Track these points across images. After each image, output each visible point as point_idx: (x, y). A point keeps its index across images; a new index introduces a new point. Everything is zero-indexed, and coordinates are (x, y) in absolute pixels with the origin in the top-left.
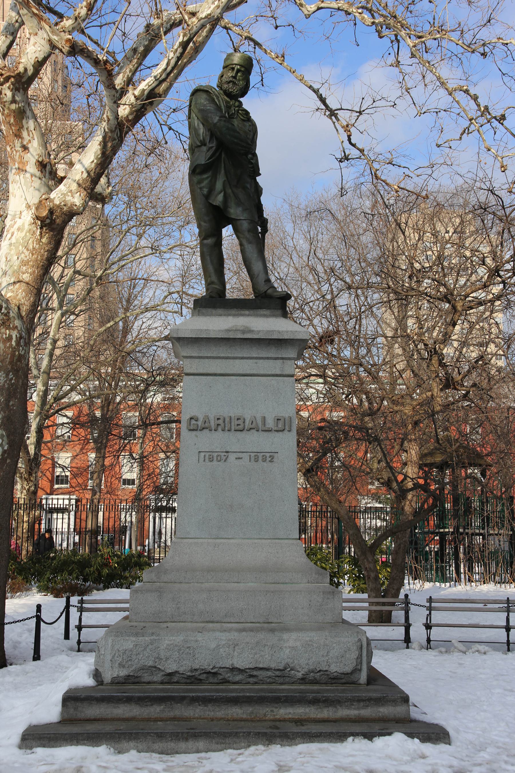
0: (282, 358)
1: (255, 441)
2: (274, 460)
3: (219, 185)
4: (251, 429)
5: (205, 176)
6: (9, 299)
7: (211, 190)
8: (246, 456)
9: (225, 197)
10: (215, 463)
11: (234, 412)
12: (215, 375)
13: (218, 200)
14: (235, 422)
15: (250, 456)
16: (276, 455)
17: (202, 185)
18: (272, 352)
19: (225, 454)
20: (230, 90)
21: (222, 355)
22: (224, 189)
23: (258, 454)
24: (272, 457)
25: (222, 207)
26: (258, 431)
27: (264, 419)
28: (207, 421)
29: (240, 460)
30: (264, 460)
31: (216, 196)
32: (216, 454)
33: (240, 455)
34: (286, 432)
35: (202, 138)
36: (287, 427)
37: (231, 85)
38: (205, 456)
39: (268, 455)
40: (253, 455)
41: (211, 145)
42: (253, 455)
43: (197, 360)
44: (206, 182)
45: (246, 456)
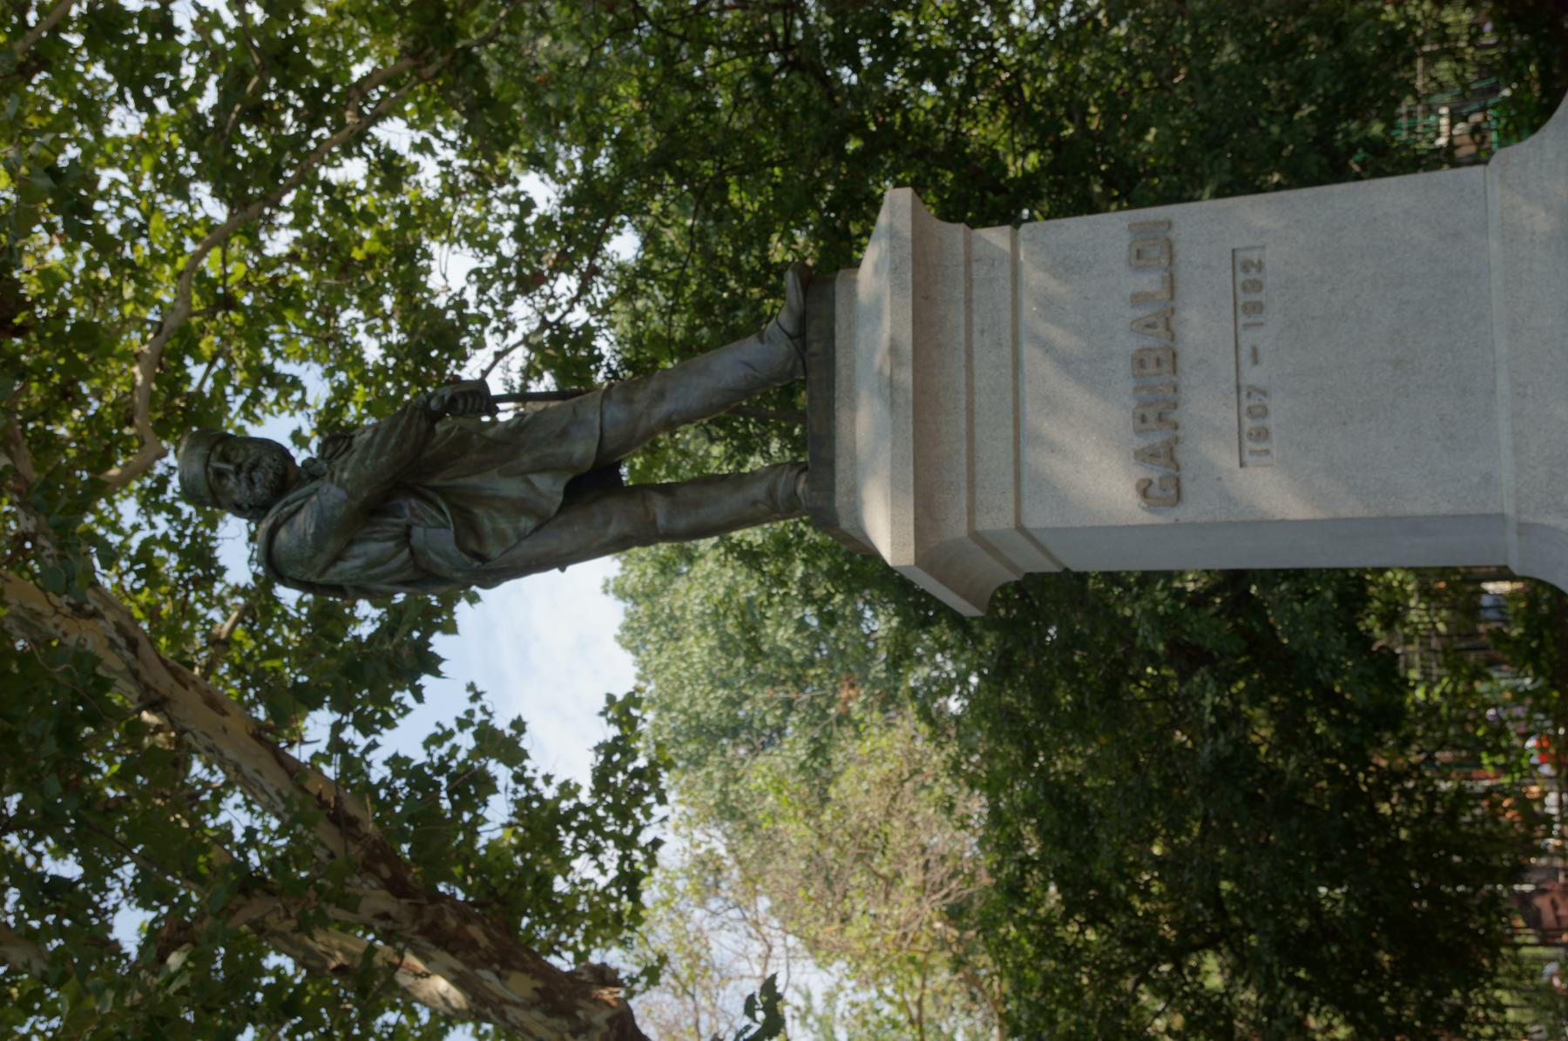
0: (968, 263)
1: (1202, 325)
3: (511, 488)
4: (1168, 328)
5: (487, 526)
6: (807, 954)
7: (521, 507)
8: (1247, 339)
9: (542, 467)
10: (1271, 422)
13: (550, 487)
15: (1246, 326)
16: (1240, 256)
17: (510, 532)
19: (1244, 394)
20: (271, 476)
21: (963, 425)
22: (524, 474)
23: (1240, 303)
24: (1246, 266)
25: (569, 477)
26: (1173, 311)
27: (1138, 299)
30: (1257, 286)
32: (1239, 292)
34: (1172, 235)
35: (391, 544)
37: (257, 475)
39: (1241, 277)
40: (1242, 319)
41: (407, 512)
42: (1242, 319)
44: (504, 525)
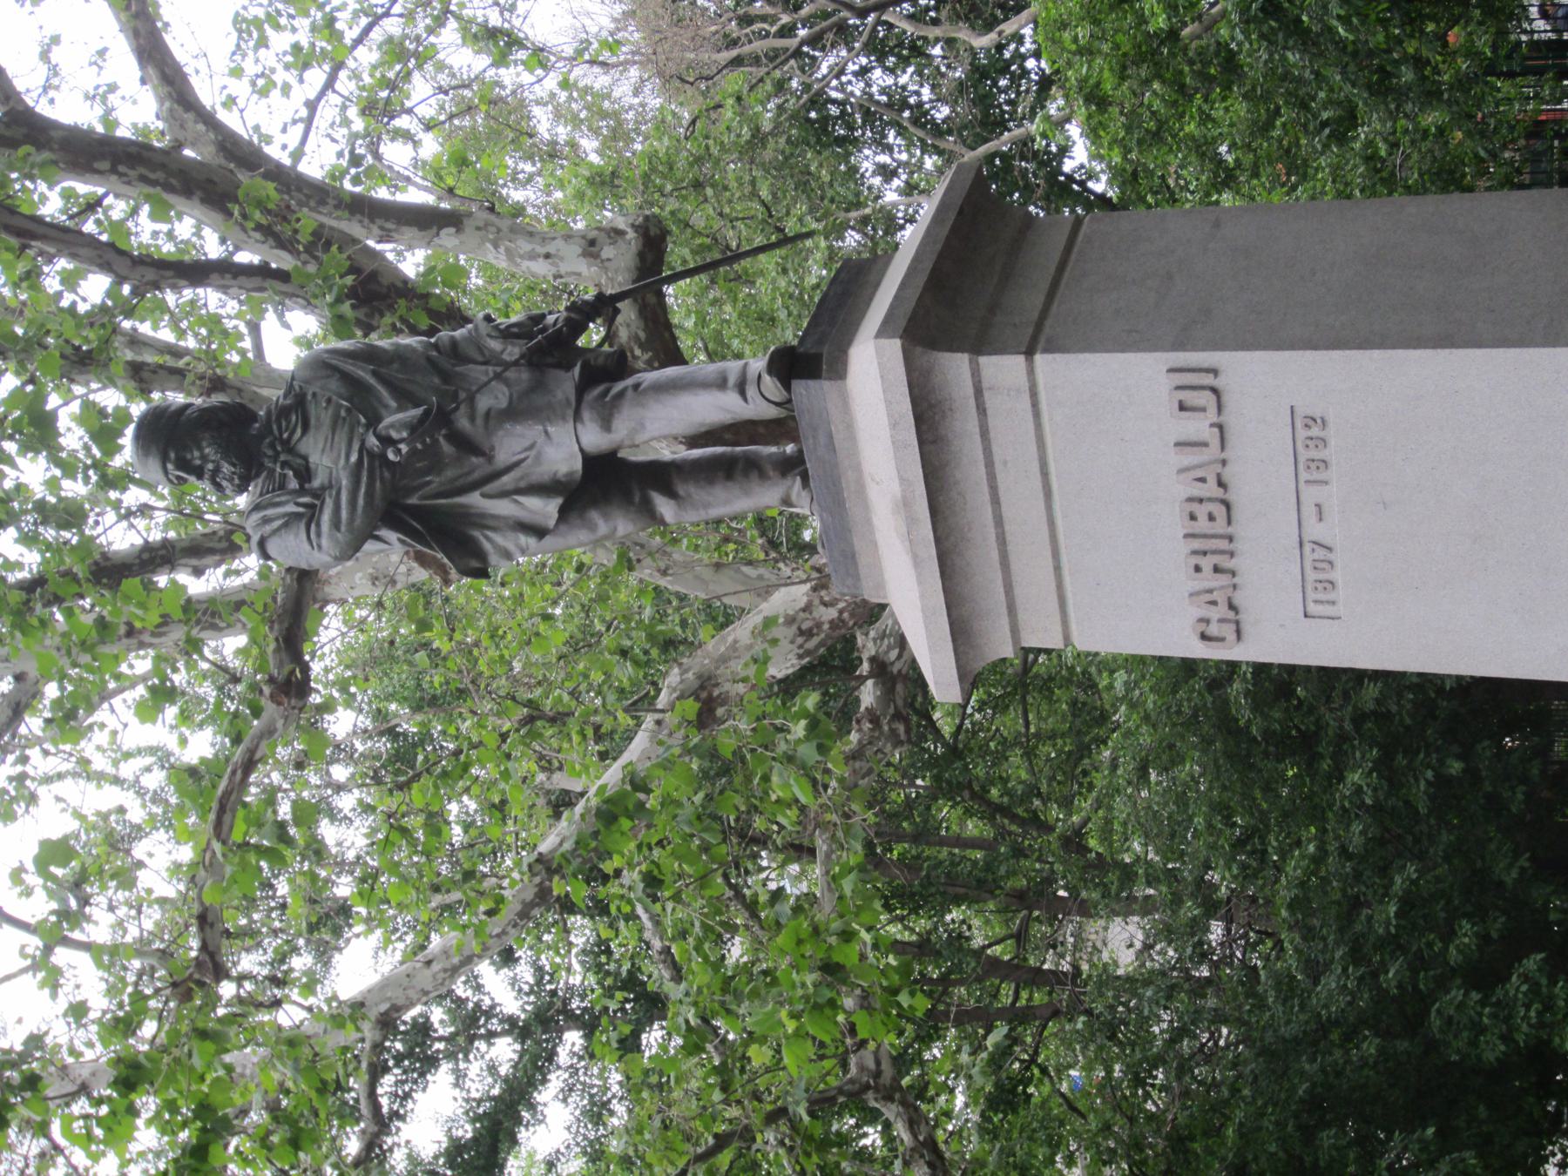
2: (1317, 415)
3: (503, 507)
5: (487, 546)
8: (1310, 495)
11: (1173, 523)
12: (1057, 569)
14: (1209, 580)
16: (1299, 413)
18: (964, 425)
23: (1302, 460)
28: (1209, 597)
29: (1325, 509)
31: (531, 511)
33: (1309, 511)
36: (1208, 380)
38: (1316, 602)
43: (1022, 616)
45: (1310, 495)
